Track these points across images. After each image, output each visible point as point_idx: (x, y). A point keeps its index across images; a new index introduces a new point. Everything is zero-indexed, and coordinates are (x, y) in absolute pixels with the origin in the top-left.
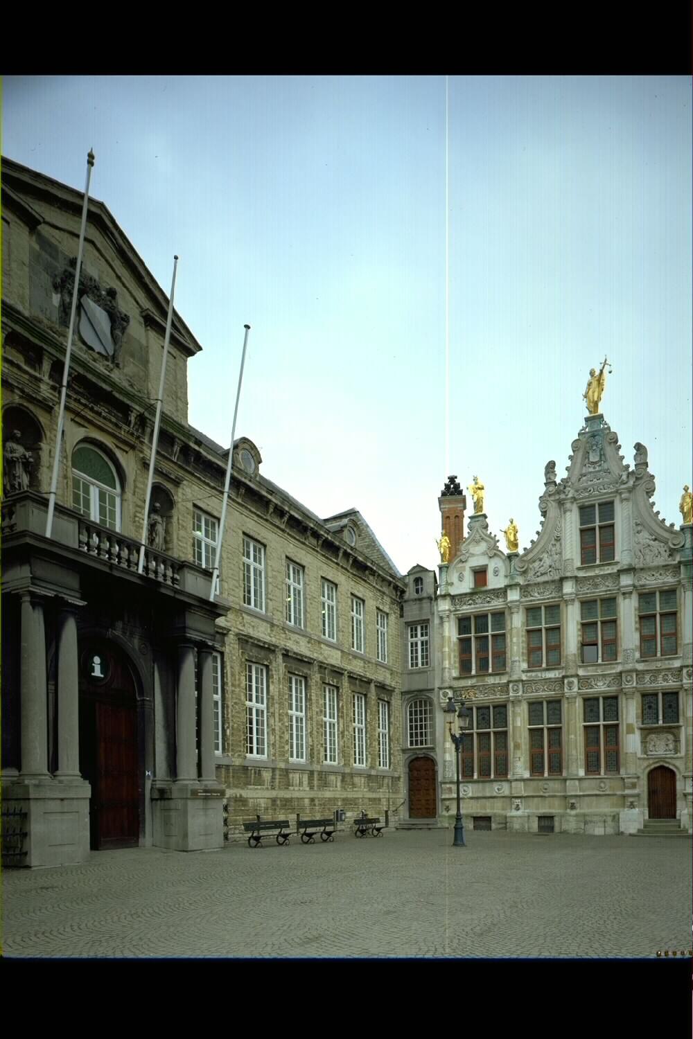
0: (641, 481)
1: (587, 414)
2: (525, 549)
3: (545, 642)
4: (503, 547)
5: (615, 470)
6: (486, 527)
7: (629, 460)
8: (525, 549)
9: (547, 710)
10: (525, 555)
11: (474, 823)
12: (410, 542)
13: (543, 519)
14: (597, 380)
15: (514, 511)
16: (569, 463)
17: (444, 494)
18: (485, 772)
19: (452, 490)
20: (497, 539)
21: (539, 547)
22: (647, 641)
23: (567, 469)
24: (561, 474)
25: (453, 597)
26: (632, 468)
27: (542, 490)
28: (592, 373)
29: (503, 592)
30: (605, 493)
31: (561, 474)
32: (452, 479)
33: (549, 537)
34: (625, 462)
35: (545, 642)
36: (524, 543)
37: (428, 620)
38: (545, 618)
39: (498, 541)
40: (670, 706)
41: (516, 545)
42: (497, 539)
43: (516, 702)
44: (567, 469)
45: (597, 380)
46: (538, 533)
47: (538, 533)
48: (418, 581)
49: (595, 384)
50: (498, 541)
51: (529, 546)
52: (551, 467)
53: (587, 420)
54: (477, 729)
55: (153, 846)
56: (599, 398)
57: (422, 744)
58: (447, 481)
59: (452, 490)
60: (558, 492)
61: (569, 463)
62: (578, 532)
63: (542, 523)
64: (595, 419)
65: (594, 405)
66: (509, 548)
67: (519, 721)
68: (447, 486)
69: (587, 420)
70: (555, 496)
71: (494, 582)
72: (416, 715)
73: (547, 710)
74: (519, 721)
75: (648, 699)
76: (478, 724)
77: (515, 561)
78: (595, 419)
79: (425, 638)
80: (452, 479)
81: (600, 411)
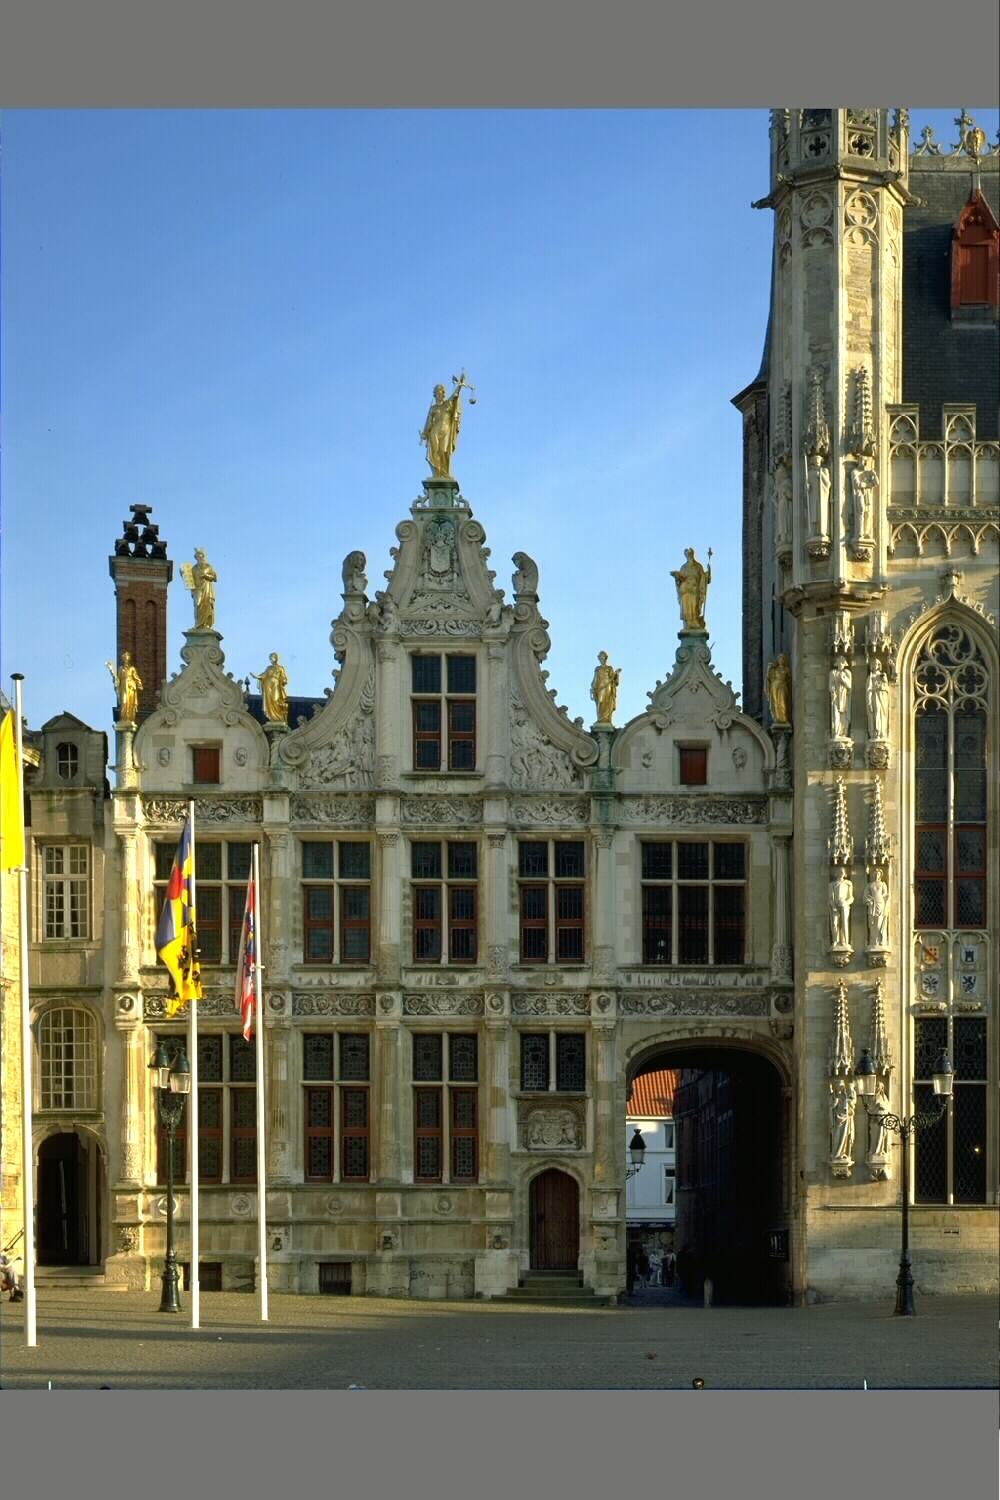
0: (526, 630)
1: (428, 475)
7: (504, 580)
13: (338, 667)
17: (121, 550)
24: (375, 583)
26: (509, 600)
28: (438, 392)
31: (375, 583)
34: (497, 584)
40: (571, 1059)
58: (130, 517)
64: (440, 487)
68: (131, 533)
75: (532, 1045)
78: (440, 487)
79: (78, 877)
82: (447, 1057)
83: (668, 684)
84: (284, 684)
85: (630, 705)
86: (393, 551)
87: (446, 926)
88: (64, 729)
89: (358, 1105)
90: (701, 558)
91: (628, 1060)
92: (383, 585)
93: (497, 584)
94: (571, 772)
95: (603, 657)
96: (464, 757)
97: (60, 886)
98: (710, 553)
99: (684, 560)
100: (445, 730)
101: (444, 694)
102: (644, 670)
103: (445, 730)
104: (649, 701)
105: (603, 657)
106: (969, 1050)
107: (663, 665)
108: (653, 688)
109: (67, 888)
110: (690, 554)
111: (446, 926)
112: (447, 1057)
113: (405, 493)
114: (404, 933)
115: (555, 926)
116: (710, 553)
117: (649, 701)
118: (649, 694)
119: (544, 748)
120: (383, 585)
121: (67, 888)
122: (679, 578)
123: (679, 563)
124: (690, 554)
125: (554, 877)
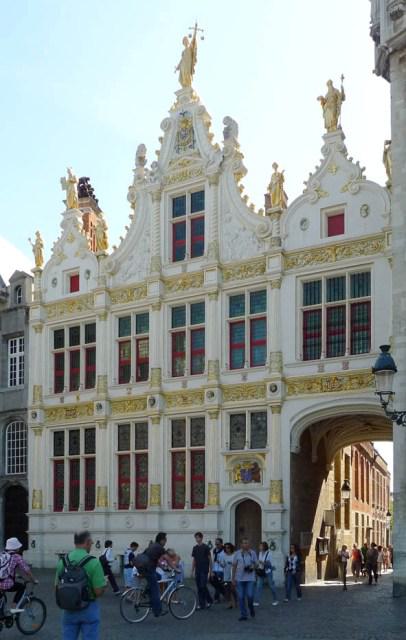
0: (230, 162)
7: (218, 139)
9: (133, 436)
10: (113, 255)
11: (85, 572)
13: (132, 212)
16: (158, 146)
20: (361, 166)
23: (158, 152)
24: (151, 158)
28: (185, 41)
29: (90, 298)
31: (151, 158)
37: (21, 334)
38: (133, 325)
39: (364, 169)
42: (361, 166)
44: (158, 152)
48: (18, 289)
50: (364, 169)
52: (142, 149)
54: (136, 449)
55: (156, 607)
57: (18, 471)
61: (158, 146)
63: (131, 217)
64: (186, 93)
72: (13, 438)
73: (133, 436)
75: (236, 422)
76: (200, 445)
77: (104, 262)
78: (186, 93)
81: (194, 85)
83: (317, 173)
84: (106, 229)
85: (294, 190)
86: (161, 139)
90: (337, 86)
91: (184, 48)
92: (155, 158)
95: (275, 166)
96: (198, 250)
97: (20, 350)
98: (343, 78)
100: (187, 239)
102: (300, 166)
103: (187, 239)
105: (275, 166)
106: (238, 430)
107: (313, 159)
108: (307, 179)
110: (330, 83)
111: (187, 351)
113: (164, 104)
114: (402, 488)
115: (247, 343)
116: (343, 78)
118: (305, 183)
120: (155, 158)
122: (323, 101)
123: (324, 92)
124: (330, 83)
125: (248, 307)
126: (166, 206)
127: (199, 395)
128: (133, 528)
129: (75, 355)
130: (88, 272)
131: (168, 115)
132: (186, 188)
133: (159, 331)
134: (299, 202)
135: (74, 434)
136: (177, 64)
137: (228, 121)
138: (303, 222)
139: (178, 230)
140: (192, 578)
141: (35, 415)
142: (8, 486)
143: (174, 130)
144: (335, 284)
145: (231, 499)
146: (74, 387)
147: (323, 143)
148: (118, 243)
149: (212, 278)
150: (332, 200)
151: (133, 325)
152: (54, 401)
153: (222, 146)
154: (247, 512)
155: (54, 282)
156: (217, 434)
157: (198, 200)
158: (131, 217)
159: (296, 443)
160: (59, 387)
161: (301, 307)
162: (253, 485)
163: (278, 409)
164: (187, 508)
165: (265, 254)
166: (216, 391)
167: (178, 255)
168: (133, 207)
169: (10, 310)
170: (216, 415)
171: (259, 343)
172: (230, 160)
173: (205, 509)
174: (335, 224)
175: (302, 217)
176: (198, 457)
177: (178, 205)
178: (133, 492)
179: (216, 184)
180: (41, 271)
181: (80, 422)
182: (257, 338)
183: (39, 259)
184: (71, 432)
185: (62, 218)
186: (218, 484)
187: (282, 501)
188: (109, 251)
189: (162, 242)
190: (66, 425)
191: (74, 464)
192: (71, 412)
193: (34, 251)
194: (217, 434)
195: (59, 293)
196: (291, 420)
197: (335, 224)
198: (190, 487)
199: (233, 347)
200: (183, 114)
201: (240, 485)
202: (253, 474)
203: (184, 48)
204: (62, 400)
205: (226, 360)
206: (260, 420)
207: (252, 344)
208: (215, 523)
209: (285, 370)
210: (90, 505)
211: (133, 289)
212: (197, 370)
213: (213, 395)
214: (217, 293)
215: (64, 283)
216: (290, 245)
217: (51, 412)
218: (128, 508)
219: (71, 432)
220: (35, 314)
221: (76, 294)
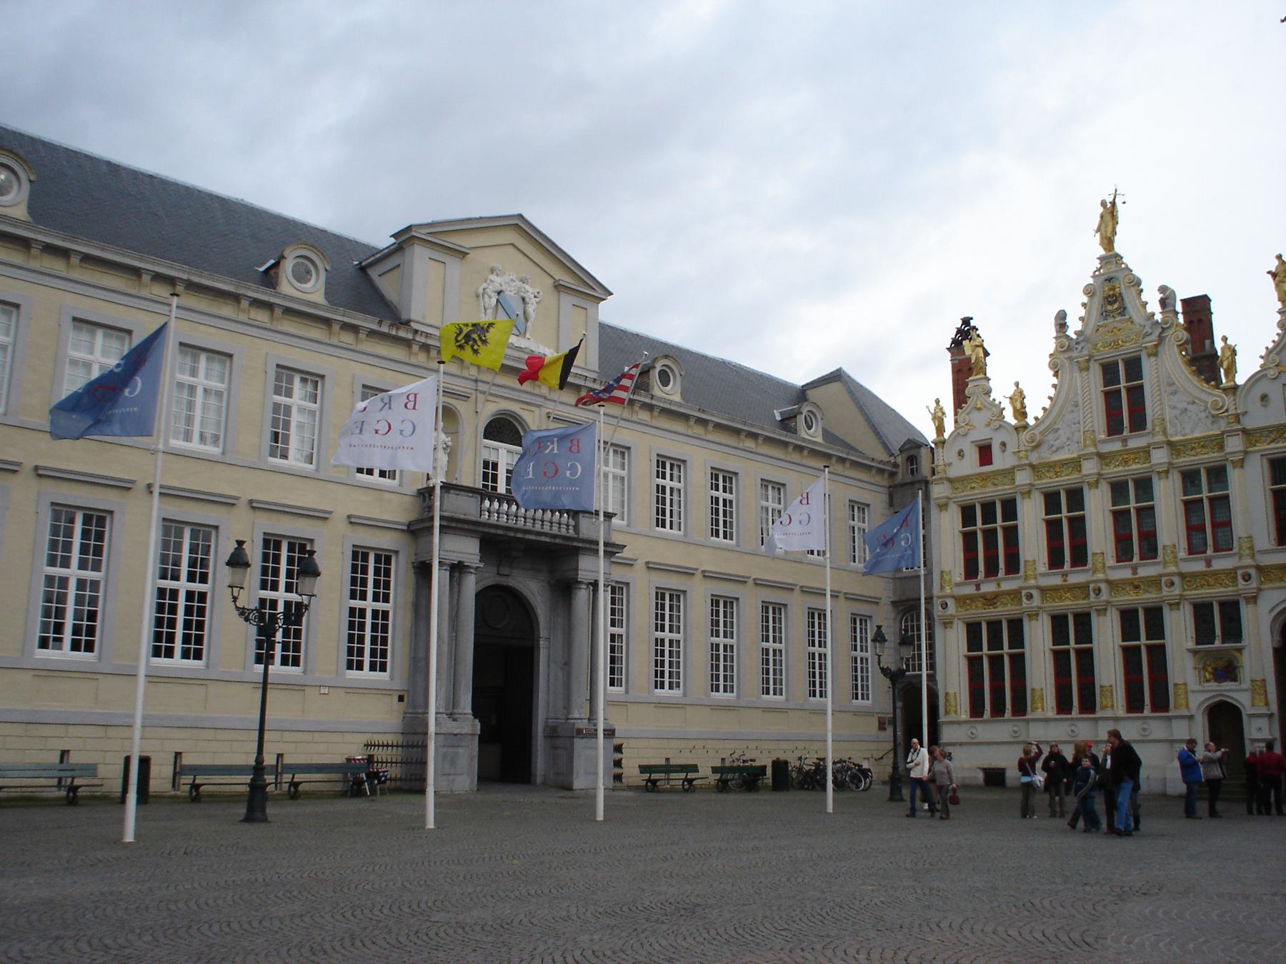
1: (1102, 252)
2: (1036, 419)
3: (1067, 543)
4: (1009, 417)
5: (1138, 319)
6: (988, 392)
7: (1154, 307)
8: (1036, 419)
9: (1072, 629)
10: (1036, 426)
12: (917, 396)
13: (1055, 381)
14: (1110, 213)
15: (1023, 373)
16: (1082, 312)
18: (998, 710)
19: (966, 331)
21: (1054, 413)
22: (1194, 529)
23: (1081, 319)
24: (1074, 326)
25: (950, 481)
26: (1158, 317)
27: (1051, 346)
28: (1103, 204)
29: (1009, 473)
30: (1128, 349)
31: (1074, 326)
32: (966, 321)
33: (1061, 404)
34: (1149, 309)
35: (1067, 543)
36: (1035, 411)
38: (1064, 505)
41: (1025, 415)
43: (1034, 615)
44: (1081, 319)
45: (1110, 213)
46: (1044, 409)
47: (1044, 409)
48: (912, 460)
49: (1108, 217)
51: (1040, 414)
53: (1101, 259)
56: (1114, 233)
59: (966, 331)
60: (1069, 349)
61: (1082, 312)
62: (1101, 399)
63: (1054, 386)
64: (1111, 258)
65: (1108, 242)
66: (1016, 418)
67: (1038, 639)
69: (1101, 259)
70: (1068, 354)
71: (1001, 461)
73: (1072, 629)
74: (1038, 639)
75: (1202, 612)
77: (1025, 436)
78: (1111, 258)
80: (966, 321)
81: (1119, 247)
82: (1142, 624)
87: (1135, 536)
88: (911, 448)
89: (1086, 658)
93: (1149, 309)
94: (1210, 419)
96: (1139, 422)
99: (1276, 263)
100: (1124, 403)
101: (1143, 641)
104: (1262, 362)
108: (1263, 353)
109: (282, 586)
111: (1135, 536)
112: (1142, 624)
117: (1262, 362)
119: (1190, 407)
121: (282, 586)
126: (1096, 374)
127: (1155, 582)
128: (1151, 738)
129: (990, 535)
130: (1004, 444)
131: (1091, 281)
132: (1118, 354)
133: (1098, 509)
134: (1254, 380)
135: (994, 626)
136: (1096, 227)
137: (1163, 289)
138: (1264, 398)
139: (1111, 399)
140: (1180, 796)
141: (945, 606)
142: (914, 681)
143: (1098, 299)
144: (988, 508)
145: (1203, 702)
146: (992, 570)
147: (1278, 317)
148: (1040, 414)
149: (1160, 457)
150: (981, 434)
151: (1064, 505)
152: (969, 590)
153: (1158, 317)
154: (1224, 718)
155: (961, 454)
156: (1179, 631)
157: (1134, 367)
158: (1054, 386)
159: (1277, 638)
160: (971, 572)
161: (1019, 522)
162: (1228, 685)
163: (1253, 599)
164: (1075, 712)
165: (1223, 433)
166: (1253, 572)
167: (1114, 428)
168: (1056, 375)
169: (902, 485)
170: (1175, 606)
171: (1223, 525)
172: (1171, 331)
173: (1170, 714)
174: (985, 453)
175: (1266, 391)
176: (1158, 653)
177: (1109, 372)
178: (1077, 690)
179: (1155, 355)
180: (943, 442)
181: (1003, 611)
182: (1221, 518)
183: (940, 429)
184: (1010, 622)
185: (1278, 317)
186: (1185, 684)
187: (1267, 704)
188: (1031, 421)
189: (1095, 414)
190: (983, 614)
191: (996, 662)
192: (991, 600)
193: (933, 419)
194: (1179, 631)
195: (970, 465)
196: (1271, 611)
197: (985, 453)
198: (1148, 686)
199: (1190, 528)
200: (1109, 280)
201: (1213, 685)
202: (1227, 671)
203: (1101, 209)
204: (978, 587)
205: (1184, 544)
206: (1231, 610)
207: (1214, 525)
208: (1188, 725)
209: (1258, 557)
210: (1020, 708)
211: (1064, 463)
212: (1224, 546)
213: (1172, 584)
214: (1167, 472)
215: (973, 455)
216: (1250, 423)
217: (961, 601)
218: (1142, 712)
219: (1010, 622)
220: (938, 491)
221: (987, 469)
